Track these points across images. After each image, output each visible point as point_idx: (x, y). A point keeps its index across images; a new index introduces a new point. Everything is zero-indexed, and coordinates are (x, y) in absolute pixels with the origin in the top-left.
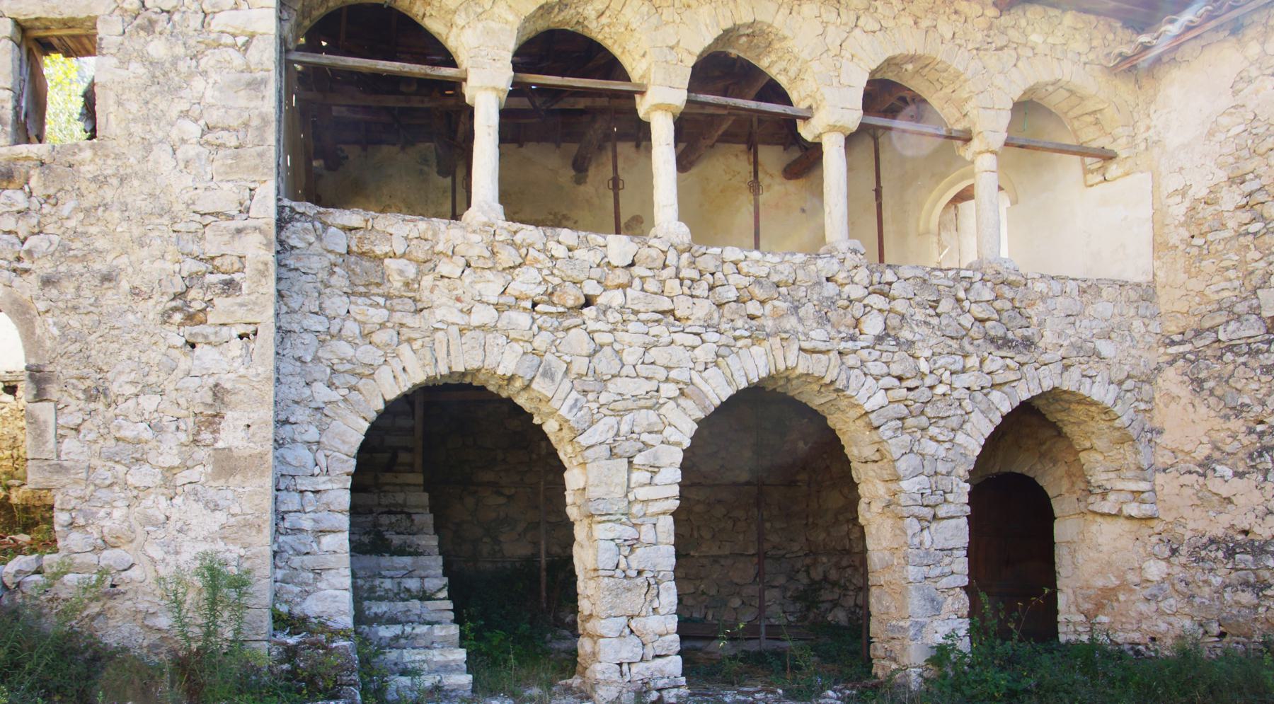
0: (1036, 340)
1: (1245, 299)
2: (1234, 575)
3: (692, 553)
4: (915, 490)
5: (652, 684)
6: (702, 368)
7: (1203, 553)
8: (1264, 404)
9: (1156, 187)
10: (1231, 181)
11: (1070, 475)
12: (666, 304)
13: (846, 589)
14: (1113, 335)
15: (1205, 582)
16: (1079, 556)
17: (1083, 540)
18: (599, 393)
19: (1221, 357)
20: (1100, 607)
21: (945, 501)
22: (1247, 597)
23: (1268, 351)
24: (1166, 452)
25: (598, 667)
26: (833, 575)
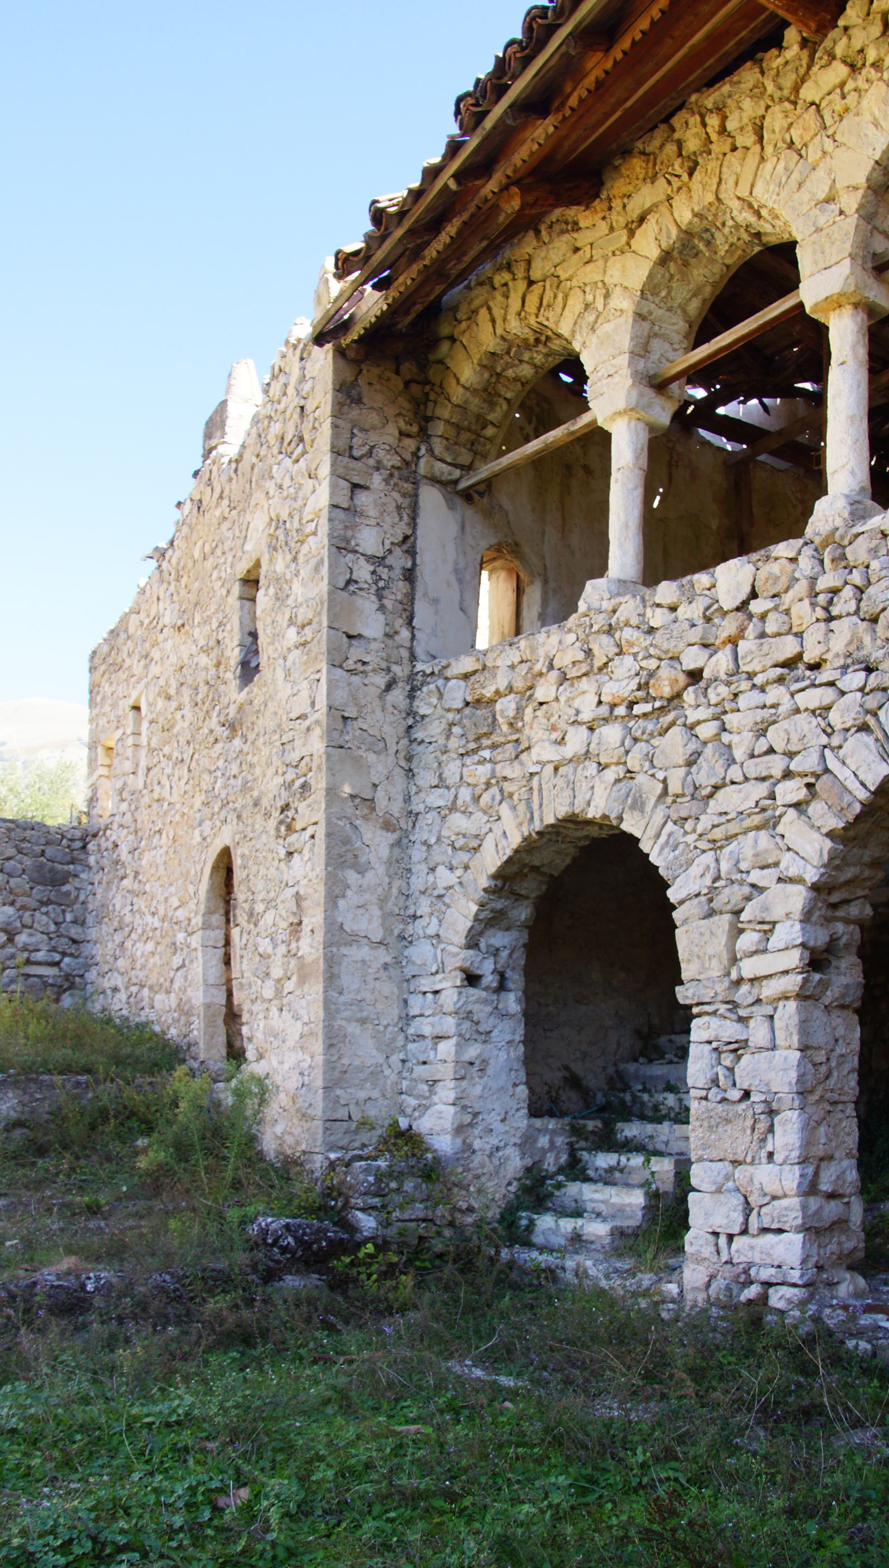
12: (788, 648)
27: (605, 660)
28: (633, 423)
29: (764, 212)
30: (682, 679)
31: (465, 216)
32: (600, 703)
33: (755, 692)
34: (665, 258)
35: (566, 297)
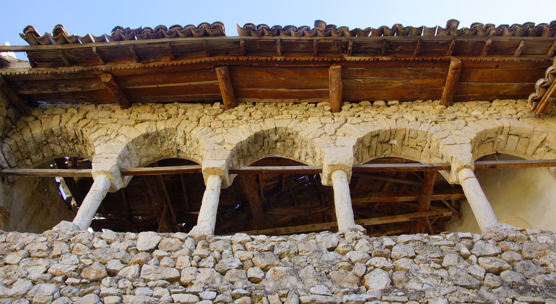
12: (174, 273)
27: (59, 253)
28: (107, 179)
29: (188, 143)
30: (104, 272)
31: (85, 69)
32: (46, 272)
33: (148, 289)
34: (146, 136)
35: (98, 129)
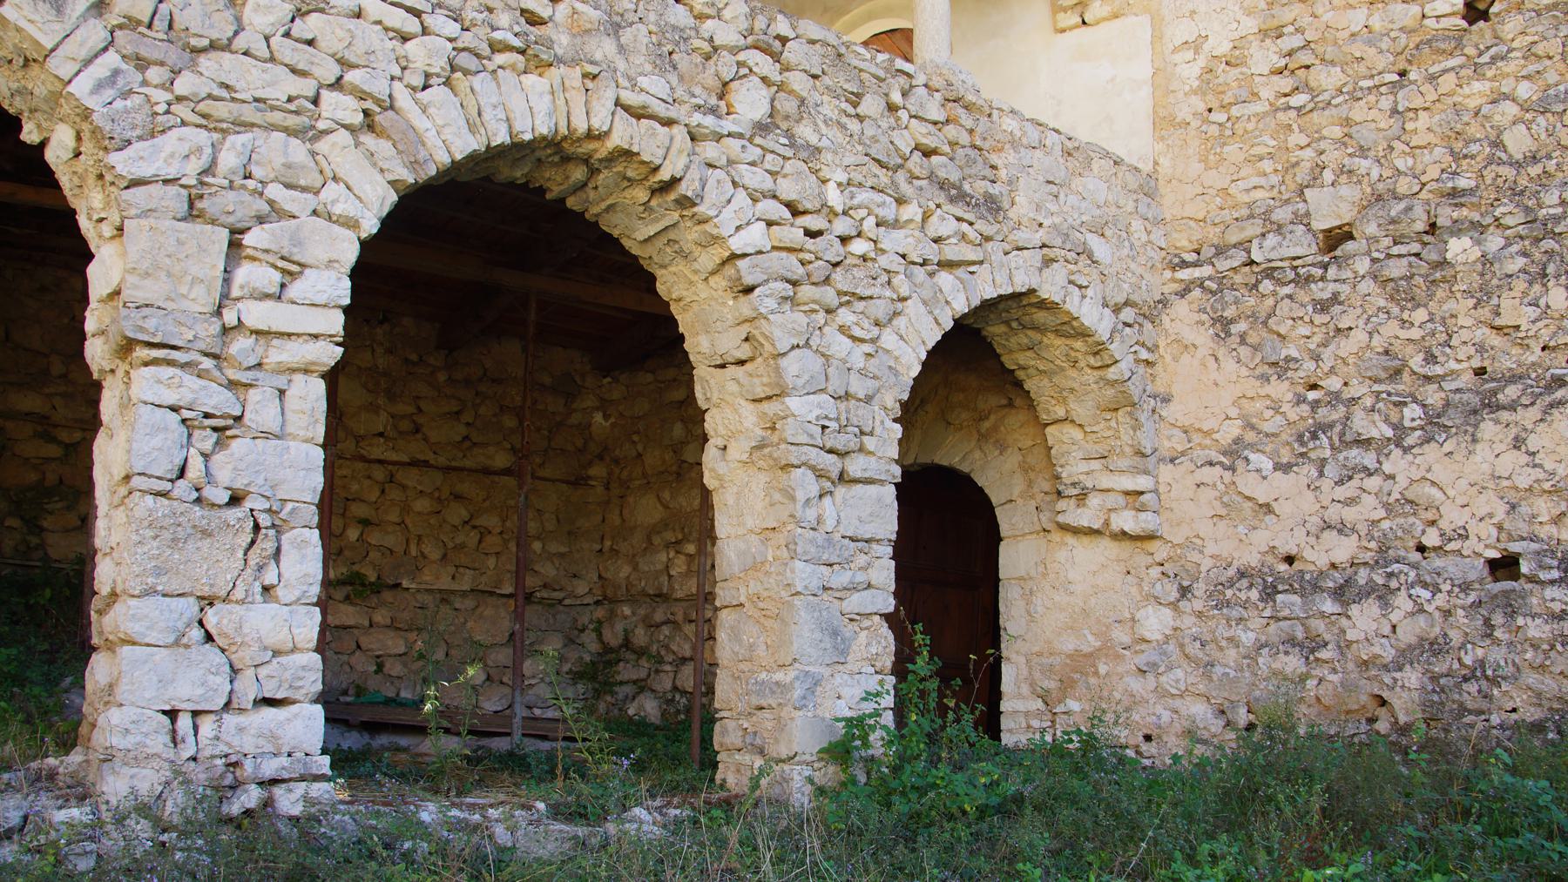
0: (1006, 205)
1: (1287, 202)
2: (1273, 627)
3: (405, 584)
4: (812, 417)
5: (248, 765)
6: (418, 81)
7: (1229, 593)
8: (1317, 358)
9: (1157, 38)
10: (1264, 33)
11: (1026, 468)
13: (661, 661)
14: (1108, 233)
15: (1230, 639)
16: (1038, 602)
17: (1045, 575)
18: (176, 72)
19: (1255, 286)
20: (1067, 686)
21: (861, 449)
22: (1292, 663)
23: (1322, 279)
24: (1176, 432)
25: (115, 716)
26: (640, 637)
